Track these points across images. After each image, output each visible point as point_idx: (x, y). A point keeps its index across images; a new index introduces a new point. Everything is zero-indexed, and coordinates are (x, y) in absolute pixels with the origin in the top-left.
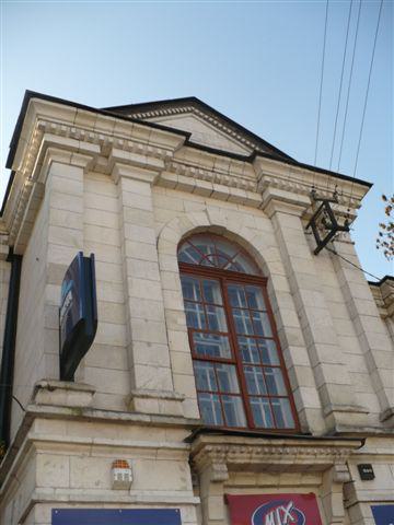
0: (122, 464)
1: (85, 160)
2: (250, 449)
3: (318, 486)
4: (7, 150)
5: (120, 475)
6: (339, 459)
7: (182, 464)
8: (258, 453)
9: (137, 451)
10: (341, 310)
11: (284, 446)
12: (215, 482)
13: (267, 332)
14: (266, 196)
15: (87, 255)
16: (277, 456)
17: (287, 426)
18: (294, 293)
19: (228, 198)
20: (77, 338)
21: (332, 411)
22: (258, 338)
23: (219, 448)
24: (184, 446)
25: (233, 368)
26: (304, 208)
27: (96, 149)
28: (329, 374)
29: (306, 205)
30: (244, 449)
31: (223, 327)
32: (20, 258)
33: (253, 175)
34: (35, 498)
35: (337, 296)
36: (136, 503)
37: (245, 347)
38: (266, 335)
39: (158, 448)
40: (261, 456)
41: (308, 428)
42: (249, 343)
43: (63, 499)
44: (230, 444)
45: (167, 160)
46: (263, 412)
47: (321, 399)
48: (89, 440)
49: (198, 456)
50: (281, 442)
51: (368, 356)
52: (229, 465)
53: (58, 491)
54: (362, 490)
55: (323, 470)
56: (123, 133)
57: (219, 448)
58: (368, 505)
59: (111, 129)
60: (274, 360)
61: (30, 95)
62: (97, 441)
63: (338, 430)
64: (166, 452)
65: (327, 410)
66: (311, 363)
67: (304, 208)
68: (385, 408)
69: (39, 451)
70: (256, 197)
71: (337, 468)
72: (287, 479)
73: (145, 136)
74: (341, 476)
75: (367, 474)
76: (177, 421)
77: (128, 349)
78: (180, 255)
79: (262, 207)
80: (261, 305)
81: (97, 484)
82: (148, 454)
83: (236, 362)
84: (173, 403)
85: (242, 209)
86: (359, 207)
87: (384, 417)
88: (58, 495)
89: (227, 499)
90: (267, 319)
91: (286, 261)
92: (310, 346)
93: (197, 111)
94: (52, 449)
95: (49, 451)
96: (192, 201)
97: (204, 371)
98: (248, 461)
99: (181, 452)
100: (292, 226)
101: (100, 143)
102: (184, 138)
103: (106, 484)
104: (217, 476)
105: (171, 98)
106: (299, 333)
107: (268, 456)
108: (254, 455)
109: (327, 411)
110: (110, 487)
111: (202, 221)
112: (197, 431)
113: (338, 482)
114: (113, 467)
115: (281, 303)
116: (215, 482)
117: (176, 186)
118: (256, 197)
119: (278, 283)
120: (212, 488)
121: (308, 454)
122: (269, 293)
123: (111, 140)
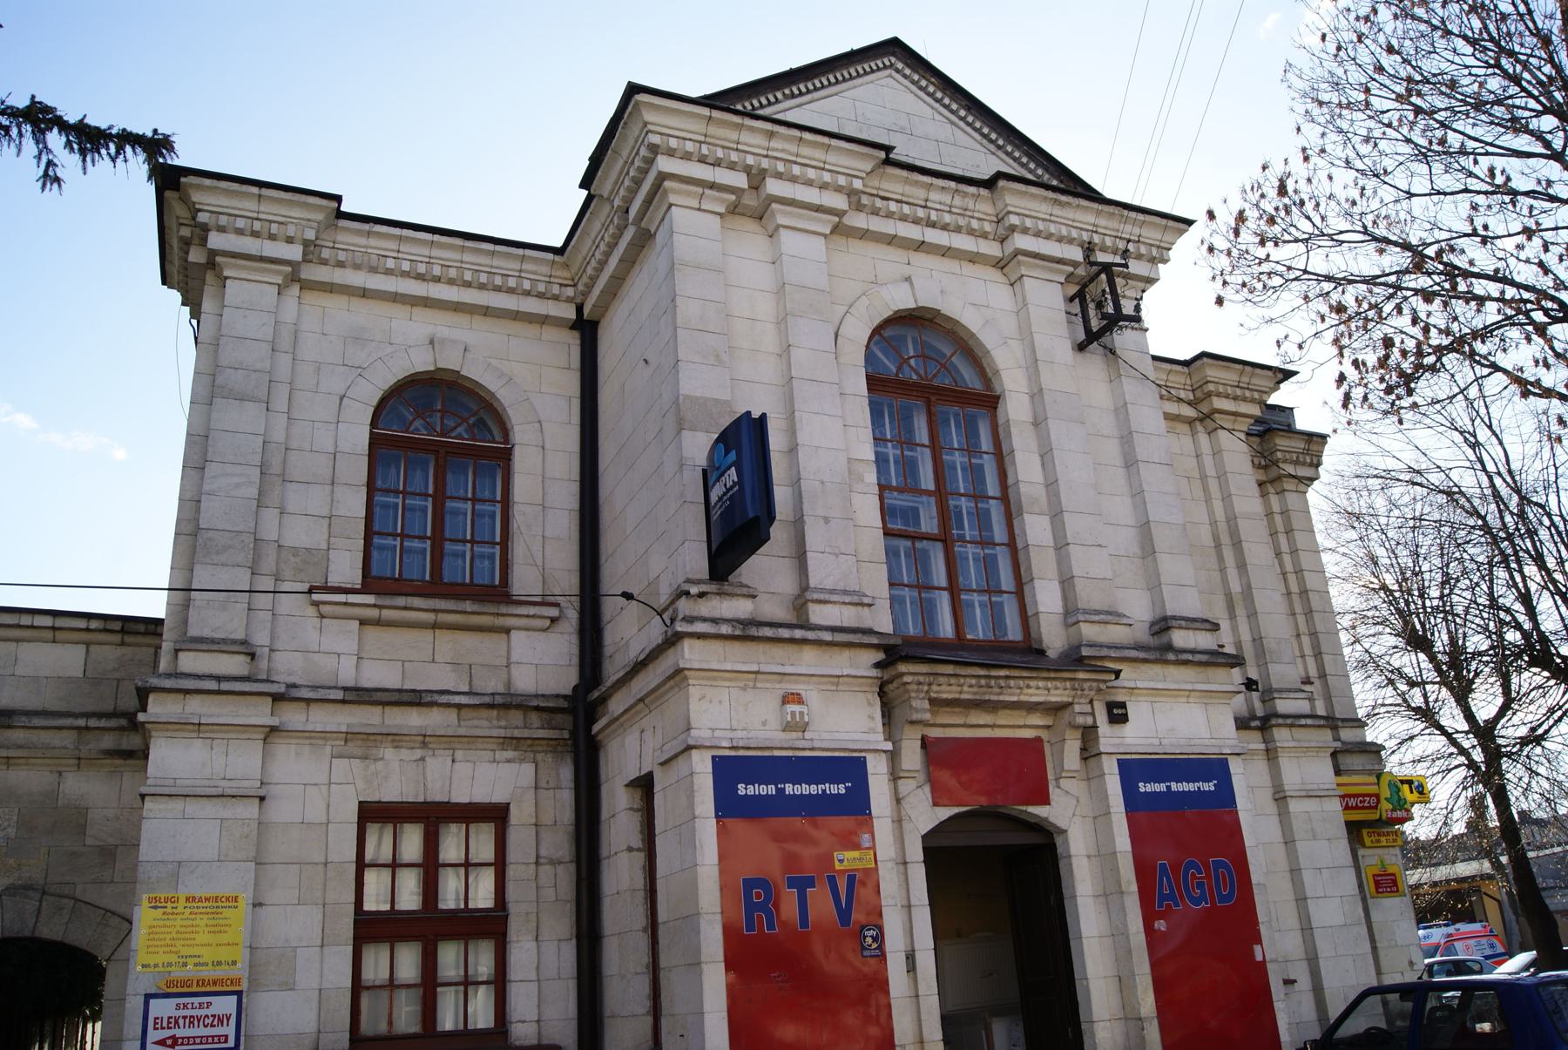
0: (798, 699)
1: (722, 201)
2: (962, 680)
3: (1048, 727)
4: (584, 164)
5: (793, 713)
6: (1081, 696)
7: (869, 696)
8: (971, 686)
9: (814, 679)
10: (1111, 451)
11: (1007, 677)
12: (912, 722)
13: (992, 488)
14: (1009, 249)
15: (756, 414)
16: (997, 690)
17: (1011, 637)
18: (1038, 423)
19: (946, 252)
21: (1078, 622)
22: (978, 496)
23: (921, 679)
24: (874, 673)
25: (939, 545)
26: (1071, 269)
27: (740, 180)
28: (1083, 562)
29: (1075, 264)
30: (953, 681)
31: (927, 480)
33: (990, 210)
34: (691, 742)
35: (1107, 424)
36: (812, 749)
37: (956, 507)
38: (991, 494)
39: (839, 677)
40: (975, 689)
41: (1041, 641)
42: (964, 503)
43: (725, 744)
45: (851, 193)
46: (978, 611)
47: (1065, 598)
48: (755, 668)
49: (891, 686)
50: (1003, 673)
52: (932, 701)
53: (717, 734)
54: (1110, 738)
55: (1057, 709)
56: (783, 151)
57: (921, 679)
58: (1115, 758)
59: (766, 144)
60: (999, 534)
61: (633, 90)
63: (1085, 652)
64: (850, 680)
65: (1071, 613)
66: (1045, 478)
67: (1071, 269)
68: (1159, 614)
69: (691, 682)
70: (991, 249)
71: (1077, 708)
72: (1003, 718)
73: (819, 154)
74: (1080, 720)
75: (1117, 714)
76: (866, 639)
78: (869, 358)
79: (1000, 264)
80: (986, 444)
81: (764, 723)
82: (826, 683)
83: (945, 538)
84: (860, 608)
85: (968, 269)
86: (1165, 261)
87: (1156, 628)
88: (719, 738)
89: (925, 743)
90: (994, 465)
91: (1033, 366)
92: (1056, 516)
93: (900, 65)
94: (708, 679)
95: (703, 682)
96: (890, 262)
97: (898, 547)
98: (957, 696)
99: (869, 681)
101: (748, 170)
102: (882, 155)
103: (774, 723)
104: (916, 716)
106: (1040, 492)
107: (985, 689)
108: (966, 688)
109: (1071, 620)
110: (780, 728)
111: (902, 300)
112: (894, 653)
113: (1076, 727)
114: (784, 703)
115: (1017, 442)
116: (912, 722)
117: (865, 235)
118: (991, 249)
119: (1016, 408)
120: (907, 728)
121: (1038, 688)
122: (1001, 420)
123: (765, 163)
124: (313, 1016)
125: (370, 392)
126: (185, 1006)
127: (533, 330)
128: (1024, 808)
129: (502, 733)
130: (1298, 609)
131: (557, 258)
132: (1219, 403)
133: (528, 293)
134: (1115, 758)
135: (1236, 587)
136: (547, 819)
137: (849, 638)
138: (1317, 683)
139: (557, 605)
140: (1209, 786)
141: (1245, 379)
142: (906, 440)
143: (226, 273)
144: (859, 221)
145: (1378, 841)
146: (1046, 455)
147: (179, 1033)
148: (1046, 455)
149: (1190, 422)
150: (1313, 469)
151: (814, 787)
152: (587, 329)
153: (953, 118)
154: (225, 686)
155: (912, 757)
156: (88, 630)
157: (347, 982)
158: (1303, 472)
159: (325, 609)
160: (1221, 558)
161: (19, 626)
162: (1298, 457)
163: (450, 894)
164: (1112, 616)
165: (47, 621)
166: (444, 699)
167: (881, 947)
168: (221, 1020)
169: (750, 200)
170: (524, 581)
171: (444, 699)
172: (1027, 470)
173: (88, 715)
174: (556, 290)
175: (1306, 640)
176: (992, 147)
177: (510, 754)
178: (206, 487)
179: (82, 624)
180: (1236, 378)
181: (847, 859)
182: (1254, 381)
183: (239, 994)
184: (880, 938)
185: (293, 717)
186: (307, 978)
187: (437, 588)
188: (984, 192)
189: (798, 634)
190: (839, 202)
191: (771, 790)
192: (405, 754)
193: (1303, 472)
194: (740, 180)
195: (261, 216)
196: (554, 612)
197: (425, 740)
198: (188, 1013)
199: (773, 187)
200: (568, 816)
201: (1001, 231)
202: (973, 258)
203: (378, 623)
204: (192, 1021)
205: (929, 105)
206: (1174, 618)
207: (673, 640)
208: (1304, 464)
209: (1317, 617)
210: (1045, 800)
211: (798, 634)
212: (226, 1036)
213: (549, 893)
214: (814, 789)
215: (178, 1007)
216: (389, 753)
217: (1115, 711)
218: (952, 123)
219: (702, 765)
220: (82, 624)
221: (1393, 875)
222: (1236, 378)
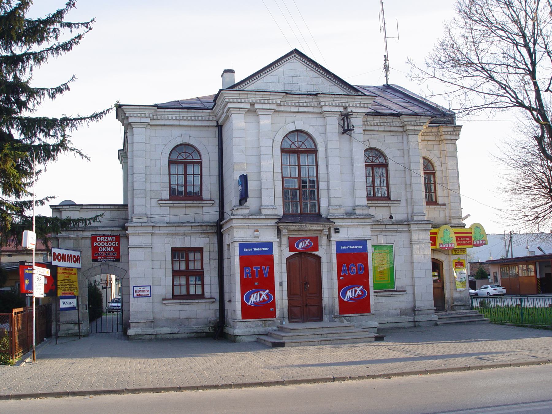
5: (256, 234)
7: (275, 229)
20: (244, 197)
27: (248, 106)
32: (221, 126)
34: (234, 241)
44: (288, 225)
52: (288, 230)
58: (335, 241)
77: (260, 190)
79: (321, 113)
92: (328, 181)
96: (289, 118)
100: (333, 123)
101: (250, 103)
104: (285, 234)
105: (283, 55)
116: (284, 235)
126: (141, 288)
127: (206, 129)
128: (311, 252)
129: (201, 231)
131: (211, 111)
132: (408, 128)
134: (335, 241)
135: (408, 183)
137: (268, 217)
143: (133, 126)
144: (281, 109)
145: (458, 253)
147: (140, 293)
149: (402, 132)
150: (458, 136)
151: (261, 249)
152: (220, 128)
153: (312, 69)
156: (111, 208)
158: (453, 137)
159: (161, 205)
161: (97, 208)
162: (451, 133)
165: (102, 207)
168: (147, 291)
169: (252, 109)
170: (206, 196)
173: (113, 227)
177: (203, 236)
178: (134, 180)
179: (109, 207)
180: (415, 119)
182: (421, 120)
183: (150, 286)
185: (157, 230)
191: (251, 250)
192: (180, 237)
193: (453, 137)
194: (248, 106)
195: (140, 113)
196: (213, 202)
198: (141, 290)
199: (257, 106)
203: (173, 207)
204: (142, 291)
205: (306, 66)
206: (357, 206)
208: (453, 135)
210: (317, 250)
212: (494, 273)
213: (212, 266)
214: (261, 249)
215: (139, 288)
217: (336, 230)
218: (312, 70)
220: (109, 207)
221: (463, 262)
222: (415, 119)
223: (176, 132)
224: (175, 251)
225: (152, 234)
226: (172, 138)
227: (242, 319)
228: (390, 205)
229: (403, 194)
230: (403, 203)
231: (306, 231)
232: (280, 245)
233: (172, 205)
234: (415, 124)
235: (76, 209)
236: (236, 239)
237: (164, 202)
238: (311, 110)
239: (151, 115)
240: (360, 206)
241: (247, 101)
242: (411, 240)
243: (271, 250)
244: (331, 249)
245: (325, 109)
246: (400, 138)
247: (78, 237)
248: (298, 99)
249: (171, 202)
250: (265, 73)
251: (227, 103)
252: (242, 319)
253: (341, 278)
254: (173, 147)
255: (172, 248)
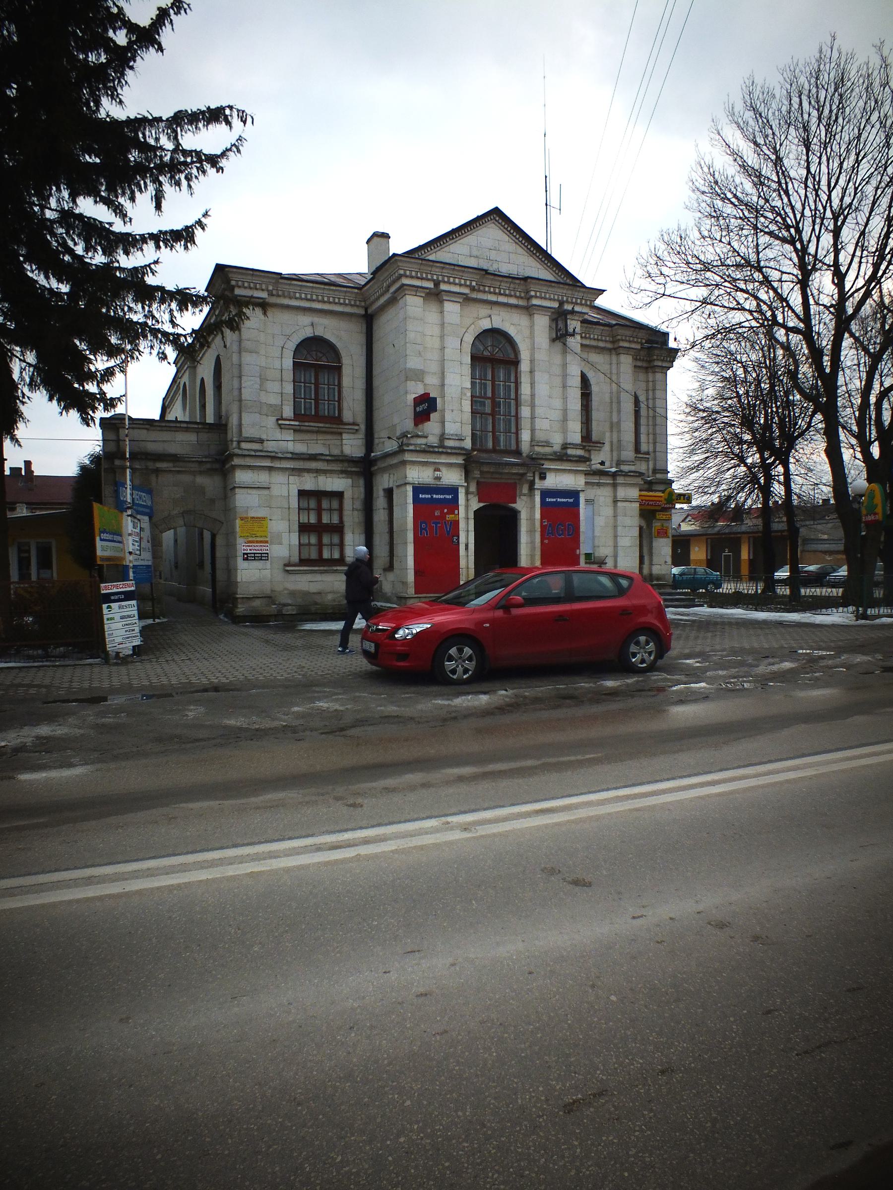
0: (439, 470)
13: (513, 396)
27: (430, 285)
48: (426, 460)
51: (565, 411)
52: (481, 471)
54: (538, 484)
62: (429, 460)
65: (533, 442)
80: (513, 379)
91: (533, 349)
92: (533, 406)
96: (484, 311)
100: (542, 322)
101: (433, 280)
111: (486, 324)
119: (524, 366)
124: (288, 552)
125: (292, 345)
129: (339, 469)
130: (651, 423)
132: (622, 344)
133: (346, 305)
135: (615, 420)
136: (356, 496)
138: (652, 454)
139: (358, 425)
140: (572, 500)
141: (635, 334)
142: (483, 378)
144: (474, 295)
146: (532, 384)
148: (532, 384)
149: (610, 350)
153: (517, 241)
154: (257, 454)
155: (473, 488)
157: (298, 543)
158: (665, 364)
159: (283, 426)
160: (611, 408)
163: (325, 520)
164: (548, 444)
166: (323, 458)
167: (458, 542)
170: (347, 416)
171: (323, 458)
172: (525, 389)
174: (358, 303)
175: (651, 436)
176: (531, 254)
177: (344, 475)
178: (243, 385)
181: (450, 517)
184: (458, 540)
186: (285, 541)
187: (317, 418)
188: (522, 282)
189: (440, 450)
190: (466, 291)
191: (430, 496)
192: (311, 475)
193: (665, 364)
196: (356, 427)
197: (318, 471)
200: (362, 496)
201: (528, 296)
202: (516, 306)
206: (570, 444)
207: (401, 451)
208: (666, 361)
209: (658, 428)
211: (440, 450)
214: (442, 497)
216: (306, 474)
218: (516, 243)
219: (410, 489)
223: (305, 320)
224: (302, 493)
225: (648, 425)
226: (298, 328)
227: (415, 594)
228: (590, 448)
229: (608, 434)
230: (607, 447)
231: (501, 474)
232: (467, 493)
233: (298, 427)
234: (631, 339)
235: (143, 426)
236: (410, 479)
237: (287, 422)
238: (513, 301)
239: (271, 288)
240: (573, 444)
241: (429, 277)
242: (615, 496)
243: (456, 499)
244: (533, 502)
245: (535, 302)
246: (607, 357)
247: (147, 468)
248: (499, 284)
249: (297, 423)
250: (453, 238)
251: (401, 276)
252: (415, 594)
253: (546, 541)
254: (300, 341)
255: (299, 491)
